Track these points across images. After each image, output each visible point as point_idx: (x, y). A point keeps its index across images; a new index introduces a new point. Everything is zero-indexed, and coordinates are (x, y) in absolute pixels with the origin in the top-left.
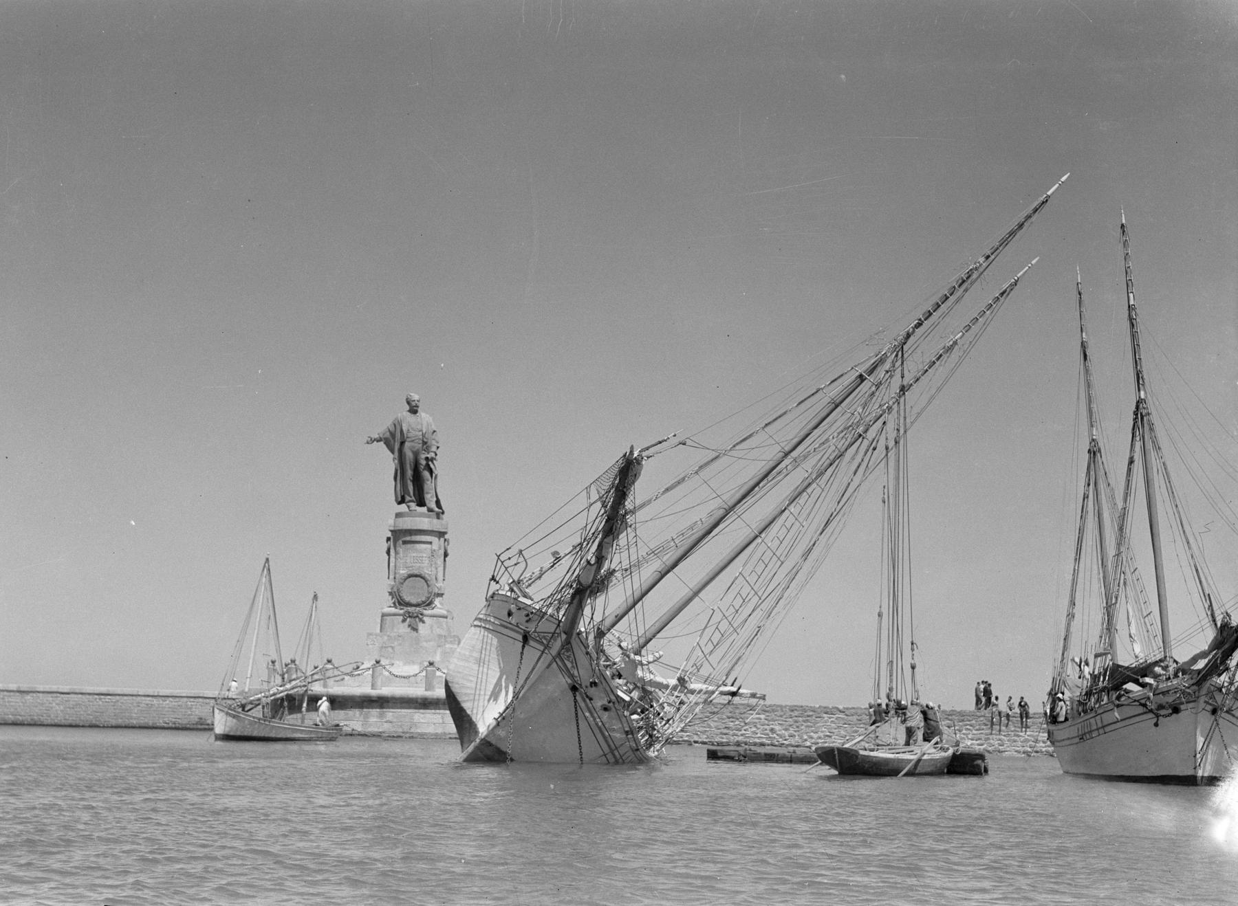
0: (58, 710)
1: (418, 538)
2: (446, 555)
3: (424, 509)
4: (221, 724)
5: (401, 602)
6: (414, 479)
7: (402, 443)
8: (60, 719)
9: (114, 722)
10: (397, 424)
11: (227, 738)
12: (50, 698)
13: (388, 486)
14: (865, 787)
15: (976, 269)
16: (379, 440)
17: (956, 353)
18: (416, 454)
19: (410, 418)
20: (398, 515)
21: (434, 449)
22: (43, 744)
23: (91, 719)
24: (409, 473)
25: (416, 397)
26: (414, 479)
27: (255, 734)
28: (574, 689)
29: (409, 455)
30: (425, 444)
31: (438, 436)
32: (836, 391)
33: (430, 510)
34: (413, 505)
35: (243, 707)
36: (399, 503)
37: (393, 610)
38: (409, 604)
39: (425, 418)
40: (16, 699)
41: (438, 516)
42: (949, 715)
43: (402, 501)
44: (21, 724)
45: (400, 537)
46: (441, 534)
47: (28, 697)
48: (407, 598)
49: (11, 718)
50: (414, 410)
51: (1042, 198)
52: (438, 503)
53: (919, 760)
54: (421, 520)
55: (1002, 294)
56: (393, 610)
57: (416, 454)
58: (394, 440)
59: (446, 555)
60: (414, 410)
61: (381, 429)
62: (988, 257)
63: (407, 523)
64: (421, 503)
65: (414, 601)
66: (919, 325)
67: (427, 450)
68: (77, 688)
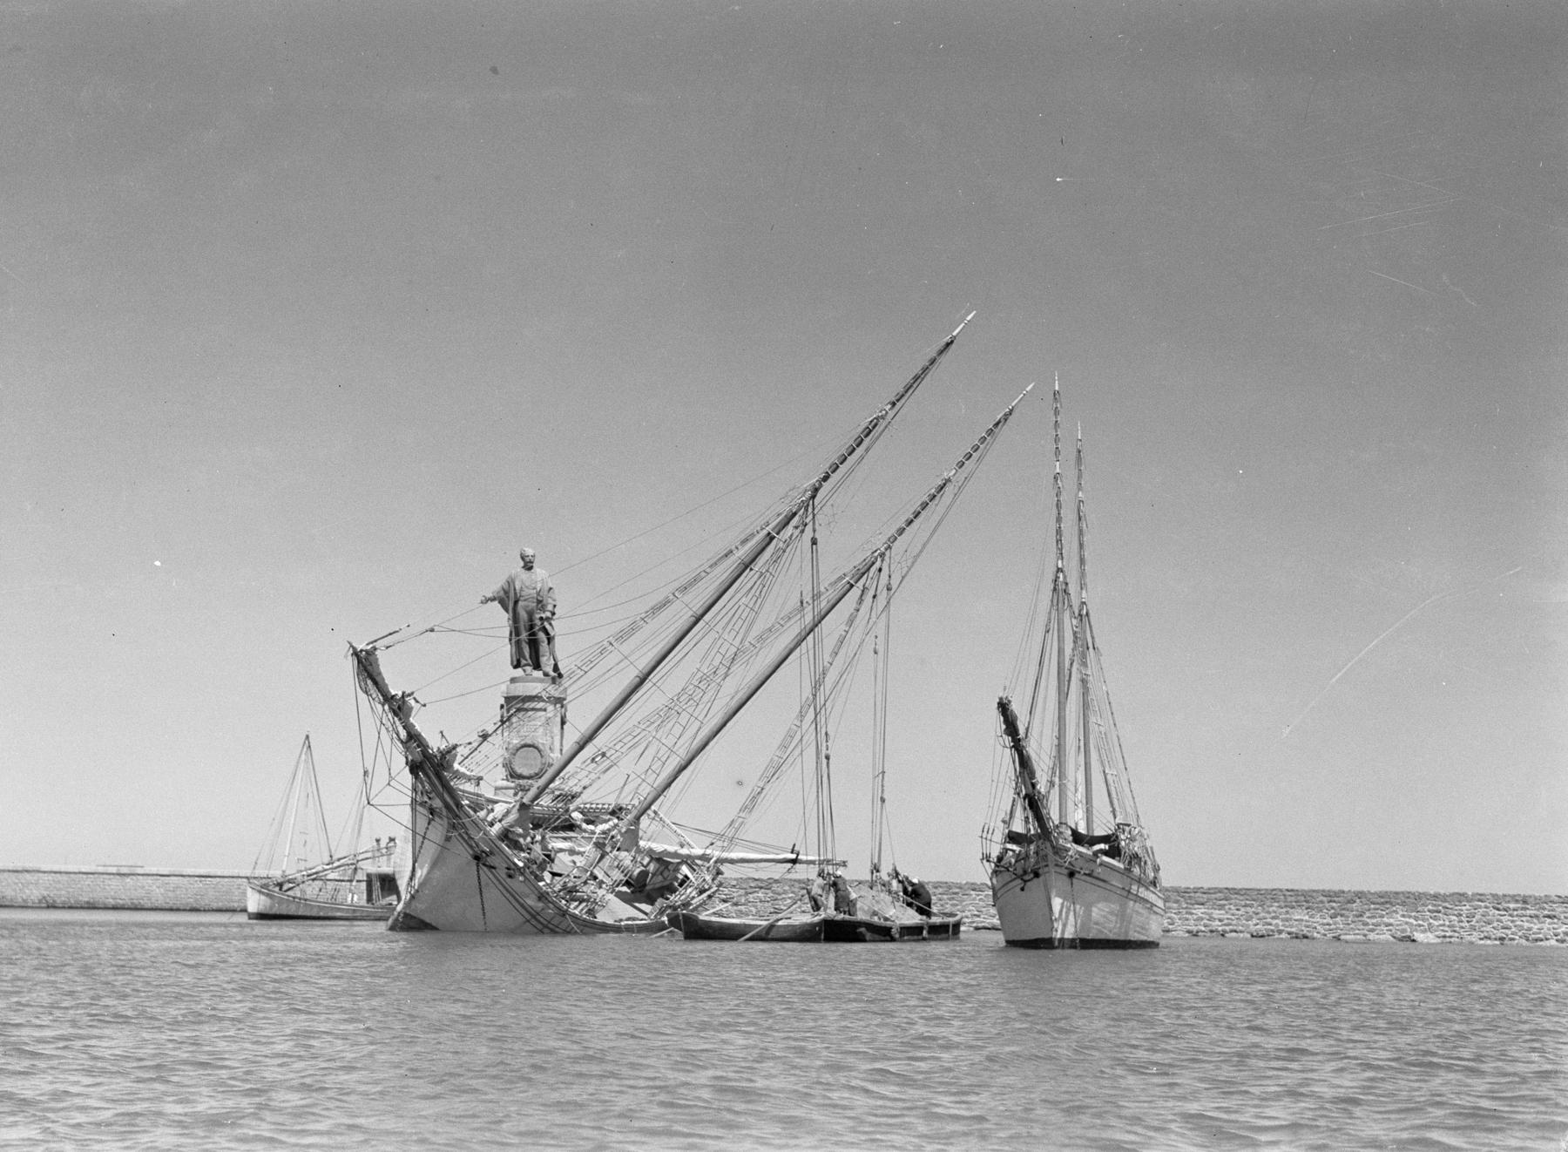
0: (158, 893)
1: (532, 705)
2: (563, 723)
3: (539, 674)
4: (255, 902)
5: (513, 775)
6: (531, 640)
7: (516, 602)
8: (160, 903)
9: (215, 905)
10: (510, 582)
11: (262, 916)
12: (149, 880)
13: (506, 651)
14: (700, 947)
15: (883, 417)
16: (493, 599)
17: (949, 489)
18: (531, 614)
19: (524, 575)
20: (513, 680)
21: (550, 608)
22: (364, 949)
23: (192, 902)
24: (524, 635)
25: (529, 552)
26: (531, 640)
27: (284, 912)
28: (477, 858)
29: (523, 615)
30: (540, 604)
31: (556, 594)
32: (743, 553)
33: (546, 674)
34: (529, 669)
35: (280, 885)
36: (515, 667)
37: (505, 783)
38: (521, 777)
39: (539, 572)
40: (115, 882)
41: (554, 681)
42: (937, 885)
43: (517, 665)
44: (178, 910)
45: (515, 705)
46: (559, 701)
47: (128, 880)
48: (519, 771)
49: (111, 902)
50: (528, 566)
51: (947, 339)
52: (556, 668)
53: (772, 926)
54: (534, 684)
55: (997, 424)
56: (505, 783)
57: (531, 614)
58: (508, 599)
59: (563, 723)
60: (528, 566)
61: (494, 586)
62: (894, 404)
63: (521, 689)
64: (537, 666)
65: (526, 772)
66: (826, 478)
67: (543, 609)
68: (178, 870)
